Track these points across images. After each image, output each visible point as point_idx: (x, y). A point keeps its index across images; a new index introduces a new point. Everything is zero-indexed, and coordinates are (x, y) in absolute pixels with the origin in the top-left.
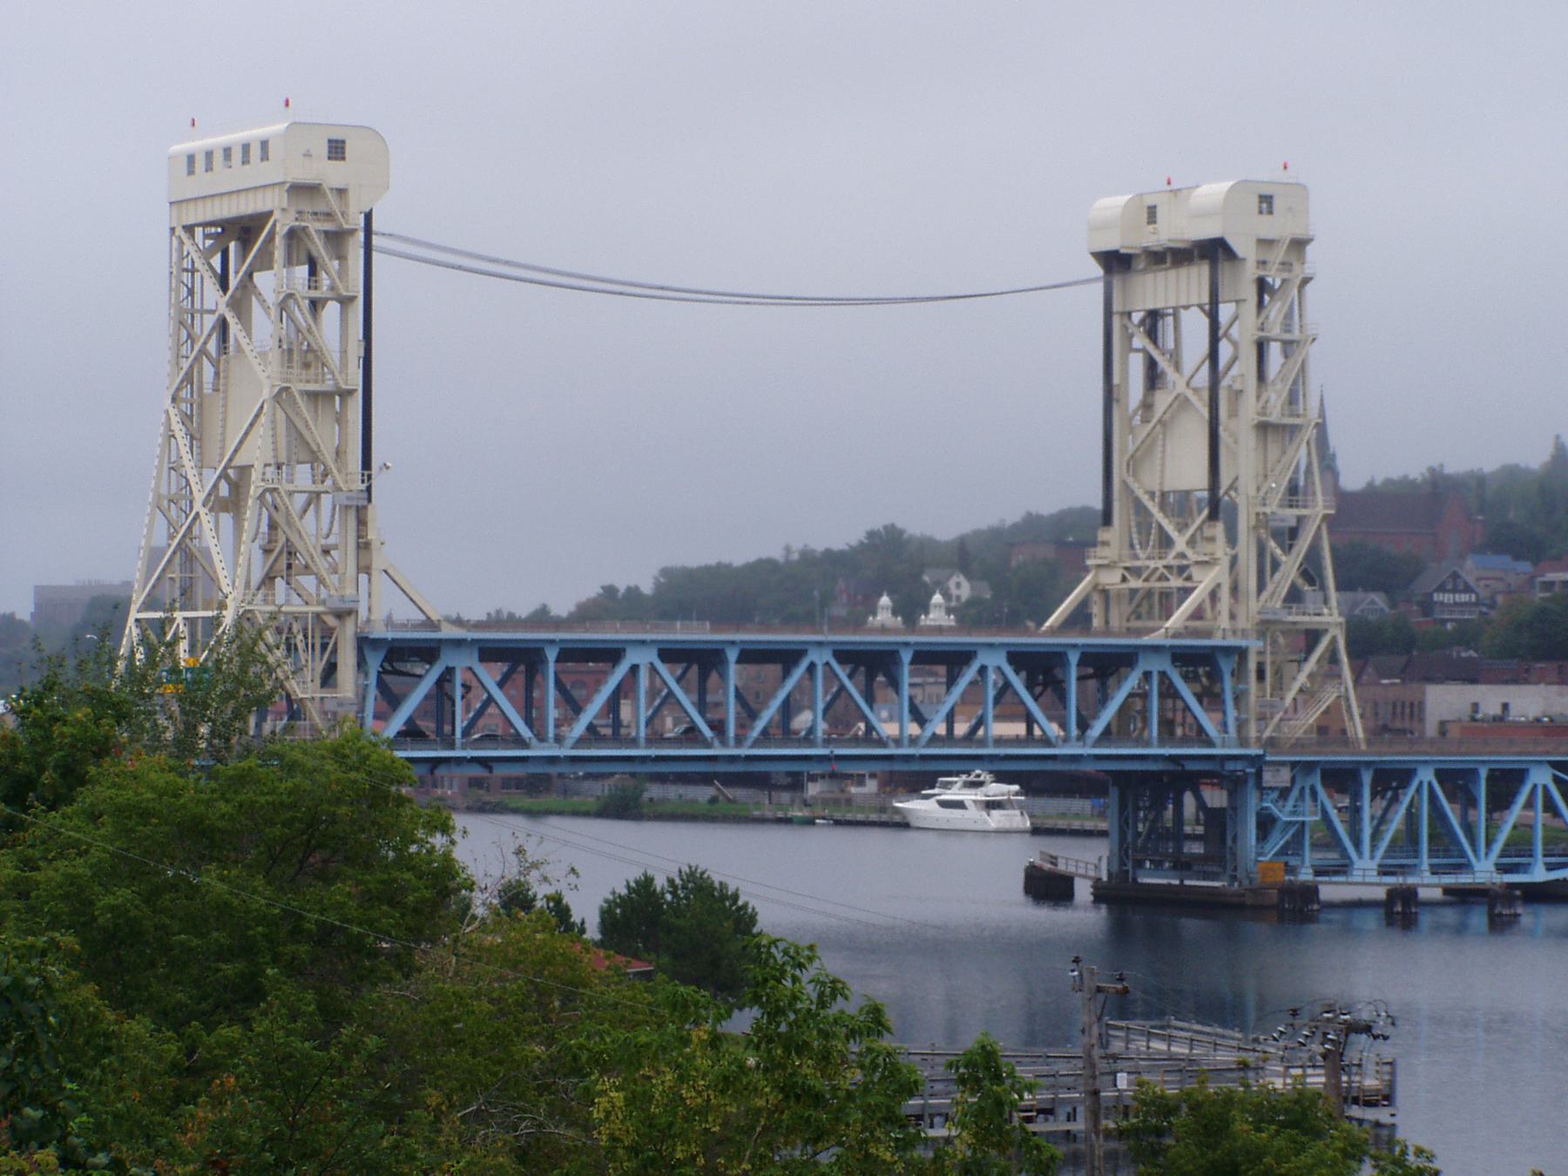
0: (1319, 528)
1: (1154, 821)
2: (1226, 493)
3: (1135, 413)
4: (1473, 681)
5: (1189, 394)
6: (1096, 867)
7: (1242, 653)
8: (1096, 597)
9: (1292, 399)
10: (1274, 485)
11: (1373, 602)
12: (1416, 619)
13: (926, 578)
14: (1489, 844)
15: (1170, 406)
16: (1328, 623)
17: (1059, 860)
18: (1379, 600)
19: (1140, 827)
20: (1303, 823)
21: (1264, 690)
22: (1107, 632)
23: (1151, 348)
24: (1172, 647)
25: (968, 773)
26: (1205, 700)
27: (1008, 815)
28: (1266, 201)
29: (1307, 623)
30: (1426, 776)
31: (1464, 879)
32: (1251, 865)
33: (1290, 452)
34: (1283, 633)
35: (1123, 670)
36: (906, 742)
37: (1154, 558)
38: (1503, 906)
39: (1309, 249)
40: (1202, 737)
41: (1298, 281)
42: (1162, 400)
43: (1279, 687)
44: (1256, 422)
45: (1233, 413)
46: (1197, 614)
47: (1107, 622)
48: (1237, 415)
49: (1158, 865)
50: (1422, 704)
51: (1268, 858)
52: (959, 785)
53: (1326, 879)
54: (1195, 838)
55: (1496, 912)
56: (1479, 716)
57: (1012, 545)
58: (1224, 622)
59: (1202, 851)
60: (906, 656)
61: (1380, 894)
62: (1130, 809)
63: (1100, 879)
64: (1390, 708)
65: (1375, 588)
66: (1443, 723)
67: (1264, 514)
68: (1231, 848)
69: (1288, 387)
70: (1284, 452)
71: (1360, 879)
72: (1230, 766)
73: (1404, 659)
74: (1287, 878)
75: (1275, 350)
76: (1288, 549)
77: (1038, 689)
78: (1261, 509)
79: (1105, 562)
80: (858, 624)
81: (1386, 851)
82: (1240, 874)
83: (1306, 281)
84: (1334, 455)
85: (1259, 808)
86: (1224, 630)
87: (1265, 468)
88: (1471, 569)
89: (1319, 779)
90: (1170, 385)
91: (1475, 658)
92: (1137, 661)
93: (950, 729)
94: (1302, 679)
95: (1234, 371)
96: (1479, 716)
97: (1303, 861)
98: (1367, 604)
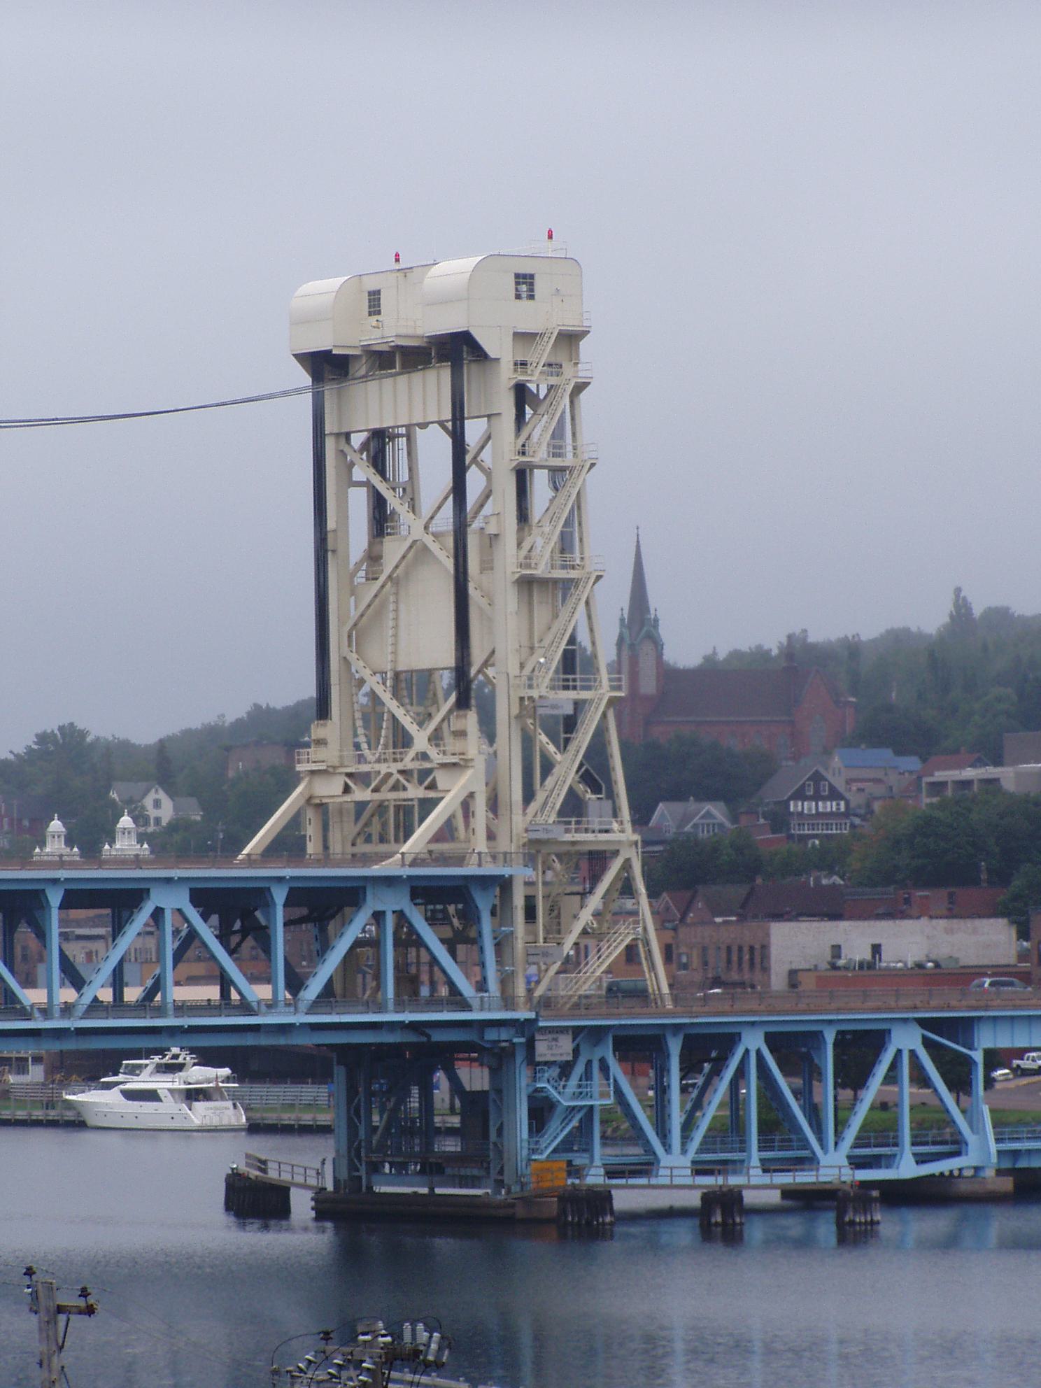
0: (604, 715)
1: (395, 1110)
2: (479, 672)
3: (358, 566)
4: (836, 916)
5: (428, 540)
6: (318, 1173)
7: (504, 885)
8: (310, 814)
9: (565, 544)
10: (542, 660)
11: (708, 815)
12: (762, 834)
13: (114, 795)
14: (838, 1134)
15: (404, 557)
16: (619, 842)
17: (270, 1165)
18: (717, 811)
19: (376, 1118)
20: (591, 1107)
21: (536, 935)
22: (326, 858)
23: (376, 480)
24: (410, 878)
25: (161, 1052)
26: (461, 949)
27: (217, 1109)
28: (525, 282)
29: (591, 842)
30: (753, 1041)
31: (804, 1178)
32: (522, 1164)
33: (564, 614)
34: (559, 856)
35: (347, 910)
36: (57, 1013)
37: (385, 760)
38: (856, 1211)
39: (583, 344)
40: (457, 999)
41: (570, 388)
42: (393, 550)
43: (556, 928)
44: (517, 576)
45: (487, 565)
46: (446, 832)
47: (326, 847)
48: (492, 569)
49: (400, 1167)
50: (765, 947)
51: (544, 1156)
52: (150, 1068)
53: (623, 1181)
54: (451, 1132)
55: (847, 1219)
56: (841, 962)
57: (228, 749)
58: (481, 844)
59: (459, 1149)
60: (55, 898)
61: (693, 1200)
62: (362, 1096)
63: (326, 1189)
64: (724, 955)
65: (711, 796)
66: (793, 973)
67: (530, 698)
68: (495, 1144)
69: (559, 528)
70: (555, 616)
71: (667, 1181)
72: (491, 1035)
73: (743, 890)
74: (569, 1181)
75: (540, 482)
76: (564, 745)
77: (235, 940)
78: (527, 693)
79: (322, 767)
80: (25, 860)
81: (701, 1144)
82: (507, 1178)
83: (579, 388)
84: (656, 620)
85: (531, 1089)
86: (480, 854)
87: (531, 637)
88: (838, 768)
89: (475, 1040)
90: (403, 530)
91: (840, 885)
92: (364, 899)
93: (118, 995)
94: (586, 916)
95: (488, 509)
96: (841, 962)
97: (592, 1159)
98: (702, 817)
